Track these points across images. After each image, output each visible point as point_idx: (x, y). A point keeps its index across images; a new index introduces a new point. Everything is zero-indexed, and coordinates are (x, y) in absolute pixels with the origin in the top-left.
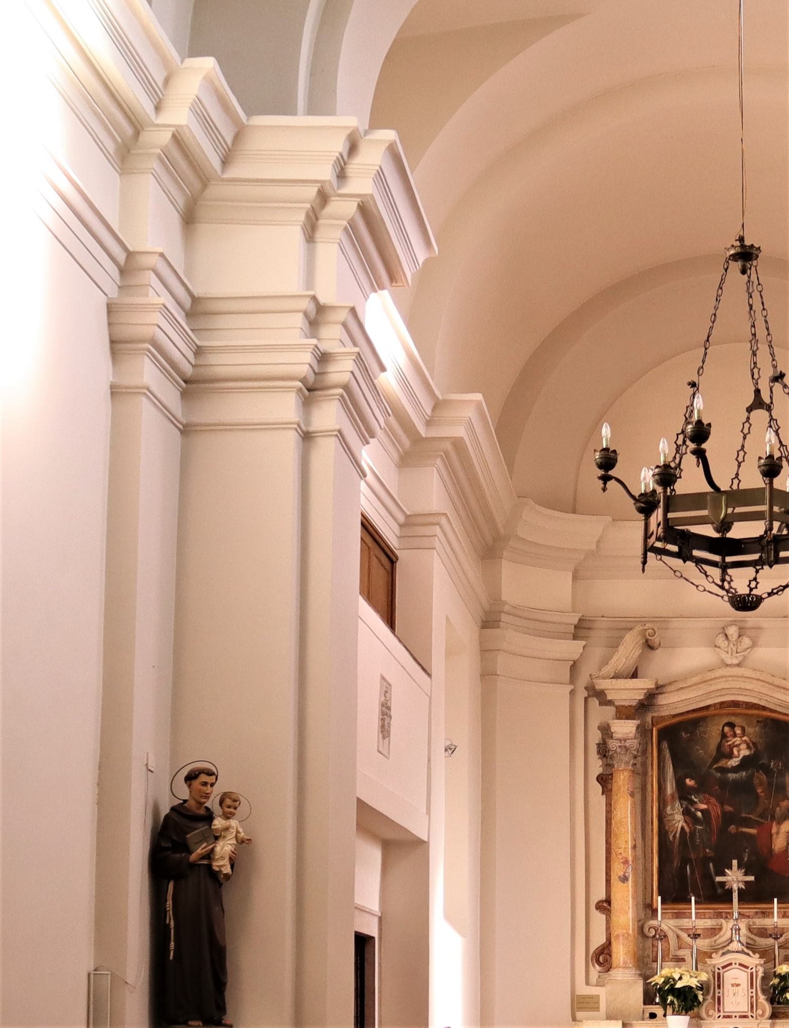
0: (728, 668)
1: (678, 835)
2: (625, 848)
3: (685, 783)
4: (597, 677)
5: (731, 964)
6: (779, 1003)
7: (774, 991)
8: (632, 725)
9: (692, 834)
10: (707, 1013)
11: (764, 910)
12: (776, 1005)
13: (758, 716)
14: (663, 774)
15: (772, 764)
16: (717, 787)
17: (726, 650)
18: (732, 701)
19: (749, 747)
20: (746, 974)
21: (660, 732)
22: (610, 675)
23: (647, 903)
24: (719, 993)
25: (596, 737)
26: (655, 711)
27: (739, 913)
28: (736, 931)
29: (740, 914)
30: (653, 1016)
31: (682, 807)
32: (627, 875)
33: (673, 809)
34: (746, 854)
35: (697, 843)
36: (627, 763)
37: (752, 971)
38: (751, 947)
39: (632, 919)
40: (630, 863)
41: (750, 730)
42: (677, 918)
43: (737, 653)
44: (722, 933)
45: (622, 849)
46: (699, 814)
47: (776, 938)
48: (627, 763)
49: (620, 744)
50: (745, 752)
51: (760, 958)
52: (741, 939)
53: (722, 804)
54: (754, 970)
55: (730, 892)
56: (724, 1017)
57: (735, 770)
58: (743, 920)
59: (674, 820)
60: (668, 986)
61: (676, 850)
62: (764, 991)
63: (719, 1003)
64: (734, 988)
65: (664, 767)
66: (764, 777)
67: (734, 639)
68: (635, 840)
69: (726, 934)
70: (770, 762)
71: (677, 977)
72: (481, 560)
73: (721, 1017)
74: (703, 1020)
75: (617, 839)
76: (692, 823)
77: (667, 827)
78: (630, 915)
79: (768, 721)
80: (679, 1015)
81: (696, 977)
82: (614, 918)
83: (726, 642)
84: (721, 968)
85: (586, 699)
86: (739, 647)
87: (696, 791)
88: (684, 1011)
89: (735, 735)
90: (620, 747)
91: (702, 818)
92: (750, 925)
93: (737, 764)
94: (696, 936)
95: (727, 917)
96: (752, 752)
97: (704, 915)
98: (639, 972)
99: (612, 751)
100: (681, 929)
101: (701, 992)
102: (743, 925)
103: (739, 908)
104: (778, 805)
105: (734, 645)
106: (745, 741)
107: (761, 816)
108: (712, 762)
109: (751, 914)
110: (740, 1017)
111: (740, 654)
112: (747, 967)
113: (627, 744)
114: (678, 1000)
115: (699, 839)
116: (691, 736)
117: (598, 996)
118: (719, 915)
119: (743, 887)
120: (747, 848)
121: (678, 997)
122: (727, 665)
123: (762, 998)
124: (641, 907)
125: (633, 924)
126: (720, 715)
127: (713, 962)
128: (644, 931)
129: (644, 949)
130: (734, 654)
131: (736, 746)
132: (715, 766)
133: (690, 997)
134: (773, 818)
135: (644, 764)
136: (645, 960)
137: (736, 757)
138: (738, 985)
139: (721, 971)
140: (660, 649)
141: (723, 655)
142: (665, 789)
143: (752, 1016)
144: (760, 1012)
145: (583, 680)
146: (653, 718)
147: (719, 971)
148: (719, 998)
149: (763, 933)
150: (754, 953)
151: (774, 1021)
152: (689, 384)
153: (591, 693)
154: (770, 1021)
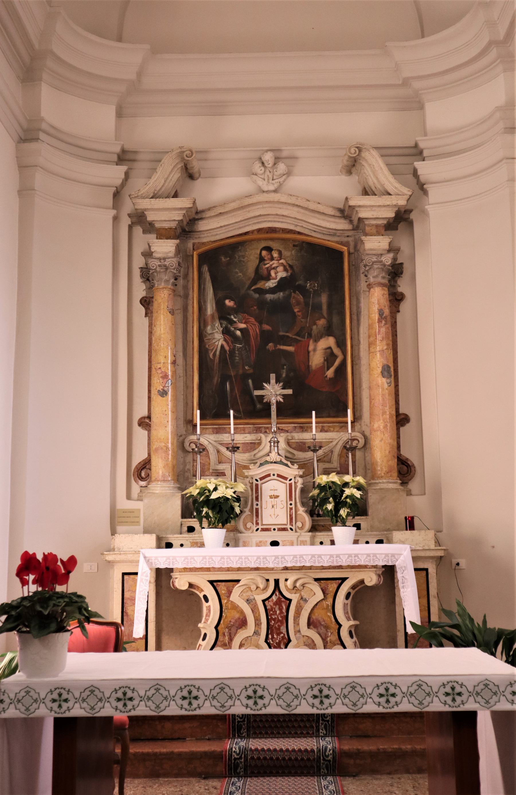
0: (265, 194)
1: (218, 353)
2: (164, 363)
3: (224, 304)
4: (135, 197)
5: (269, 475)
6: (319, 515)
7: (314, 503)
8: (171, 245)
9: (232, 352)
10: (245, 525)
11: (301, 425)
12: (316, 518)
13: (294, 240)
14: (204, 295)
15: (308, 284)
16: (255, 307)
17: (262, 177)
18: (269, 227)
19: (285, 270)
20: (284, 485)
21: (200, 256)
22: (149, 195)
23: (188, 419)
24: (257, 505)
25: (139, 262)
26: (196, 238)
27: (278, 428)
28: (274, 444)
29: (279, 429)
30: (191, 529)
31: (221, 327)
32: (166, 389)
33: (213, 328)
34: (284, 371)
35: (237, 361)
36: (167, 281)
37: (290, 482)
38: (291, 460)
39: (172, 432)
40: (170, 377)
41: (286, 253)
42: (217, 433)
43: (273, 180)
44: (261, 447)
45: (162, 364)
46: (238, 333)
47: (315, 451)
48: (167, 281)
49: (159, 263)
50: (282, 274)
51: (298, 469)
52: (280, 452)
53: (260, 323)
54: (293, 481)
55: (268, 405)
56: (263, 530)
57: (272, 291)
58: (282, 434)
59: (214, 338)
60: (203, 497)
61: (216, 367)
62: (303, 504)
63: (257, 516)
64: (273, 500)
65: (204, 288)
66: (301, 298)
67: (270, 166)
68: (175, 356)
69: (265, 446)
70: (306, 283)
71: (211, 487)
72: (21, 83)
73: (260, 529)
74: (241, 533)
75: (157, 355)
76: (232, 343)
77: (207, 346)
78: (169, 428)
79: (304, 245)
80: (216, 528)
81: (232, 488)
82: (153, 432)
83: (263, 168)
84: (259, 480)
85: (130, 227)
86: (276, 173)
87: (235, 311)
88: (220, 524)
89: (272, 259)
90: (160, 266)
91: (241, 337)
92: (288, 439)
93: (274, 285)
94: (234, 449)
95: (266, 432)
96: (289, 274)
97: (244, 430)
98: (179, 486)
99: (153, 270)
100: (221, 444)
101: (238, 504)
102: (282, 438)
103: (277, 423)
104: (315, 324)
105: (270, 172)
106: (282, 263)
107: (298, 334)
108: (251, 284)
109: (289, 428)
110: (279, 530)
111: (277, 181)
112: (285, 478)
113: (167, 263)
114: (213, 513)
115: (238, 351)
116: (230, 260)
117: (139, 510)
118: (258, 430)
119: (282, 400)
120: (286, 365)
121: (213, 509)
122: (264, 192)
123: (301, 510)
124: (181, 422)
125: (173, 439)
126: (259, 240)
127: (251, 473)
128: (185, 446)
129: (185, 464)
130: (271, 181)
131: (274, 268)
132: (253, 288)
133: (225, 508)
134: (310, 336)
135: (185, 287)
136: (187, 474)
137: (273, 279)
138: (277, 497)
139: (259, 483)
140: (200, 179)
141: (260, 182)
142: (206, 309)
143: (291, 529)
144: (299, 524)
145: (128, 207)
146: (194, 244)
147: (257, 482)
148: (257, 510)
149: (302, 447)
150: (293, 463)
151: (314, 534)
152: (278, 496)
153: (134, 220)
154: (310, 534)
